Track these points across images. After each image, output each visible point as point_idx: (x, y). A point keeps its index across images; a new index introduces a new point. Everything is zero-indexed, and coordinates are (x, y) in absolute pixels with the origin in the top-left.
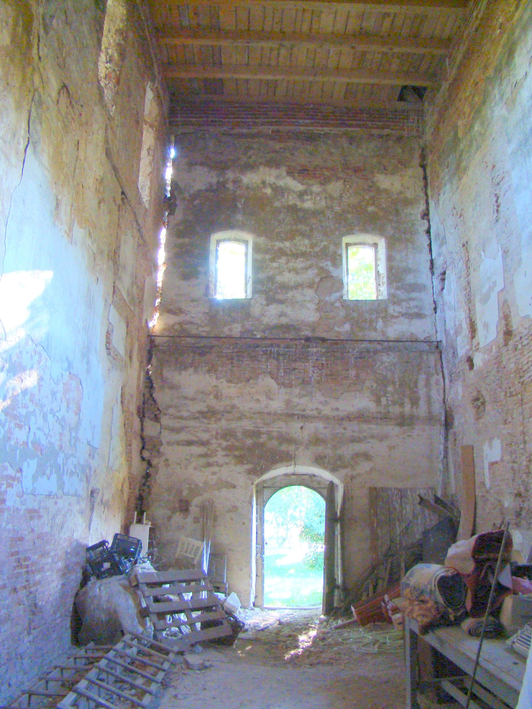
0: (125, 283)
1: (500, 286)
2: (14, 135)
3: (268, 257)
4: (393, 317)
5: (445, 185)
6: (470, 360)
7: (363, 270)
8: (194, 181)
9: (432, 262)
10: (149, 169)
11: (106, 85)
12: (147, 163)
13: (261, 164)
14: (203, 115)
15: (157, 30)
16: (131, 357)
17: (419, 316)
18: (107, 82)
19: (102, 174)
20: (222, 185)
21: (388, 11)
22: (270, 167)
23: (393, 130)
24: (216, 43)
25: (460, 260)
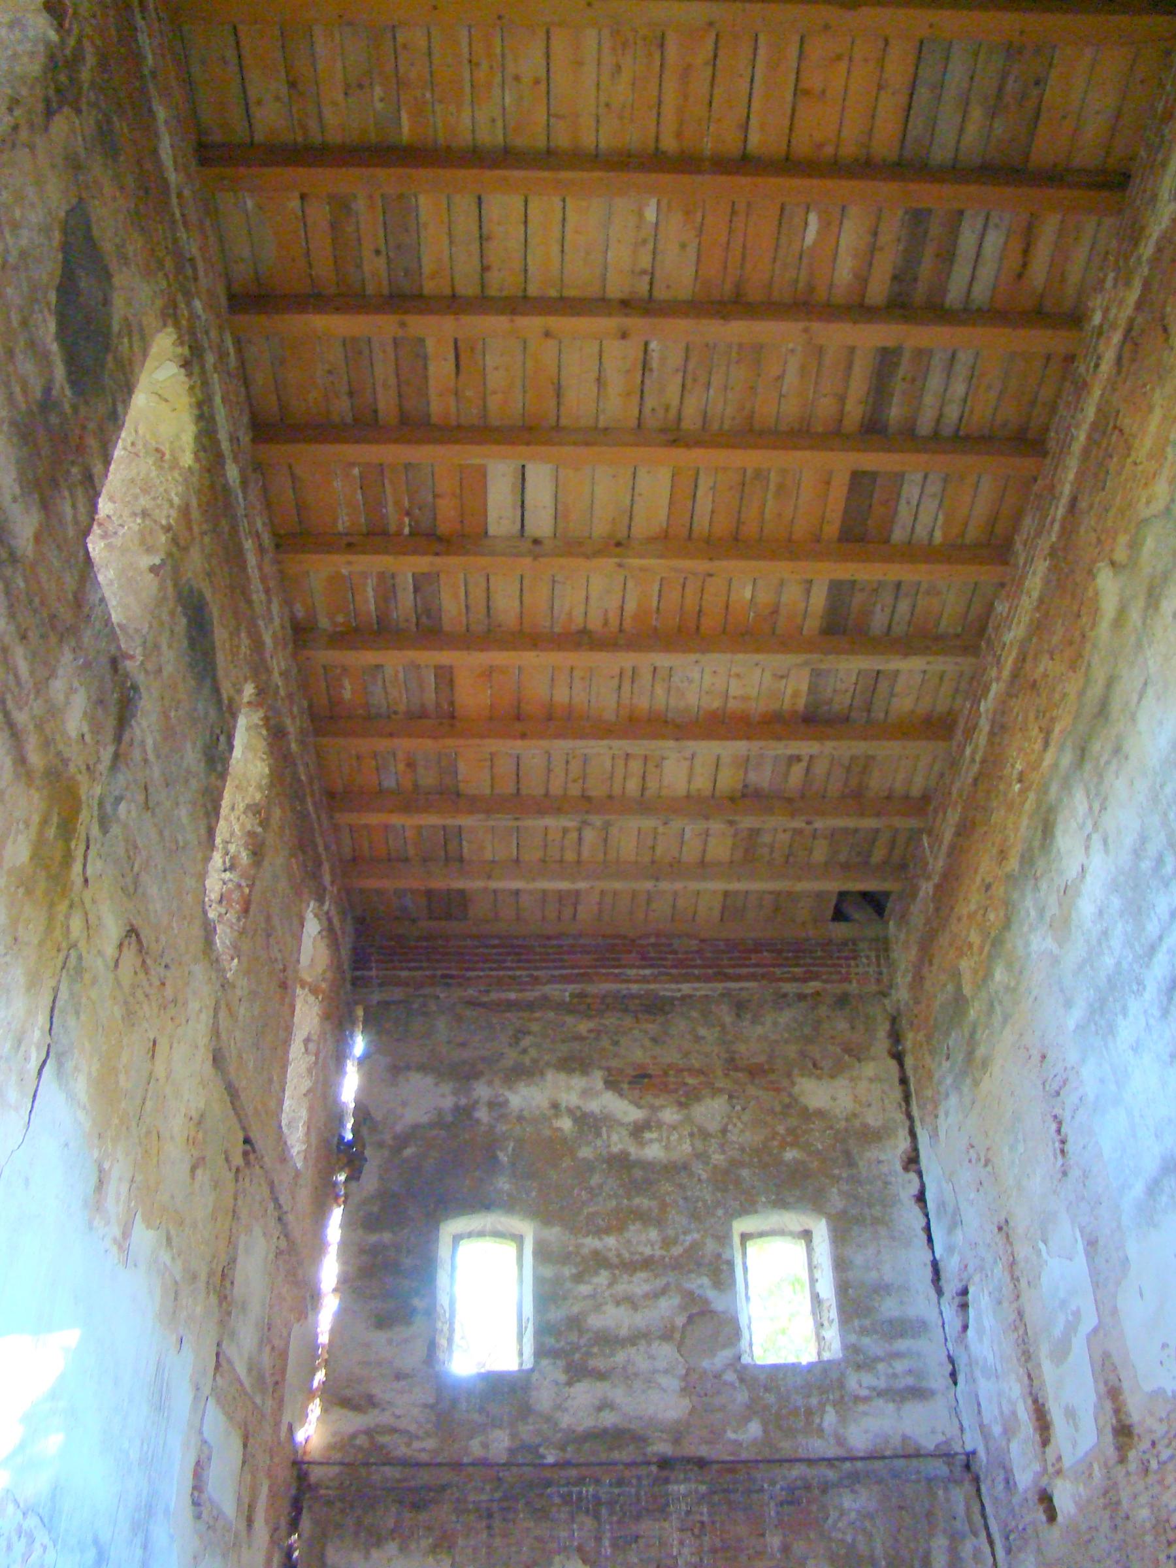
0: (245, 1341)
1: (1089, 1321)
2: (19, 1042)
3: (568, 1271)
4: (857, 1399)
5: (947, 1095)
6: (1046, 1499)
7: (781, 1296)
8: (404, 1104)
9: (935, 1264)
10: (307, 1084)
11: (220, 915)
12: (303, 1067)
13: (548, 1064)
14: (425, 964)
15: (331, 795)
16: (250, 1521)
17: (918, 1393)
18: (223, 911)
19: (202, 1105)
20: (464, 1113)
21: (796, 752)
22: (571, 1071)
23: (826, 981)
24: (449, 822)
25: (995, 1262)
